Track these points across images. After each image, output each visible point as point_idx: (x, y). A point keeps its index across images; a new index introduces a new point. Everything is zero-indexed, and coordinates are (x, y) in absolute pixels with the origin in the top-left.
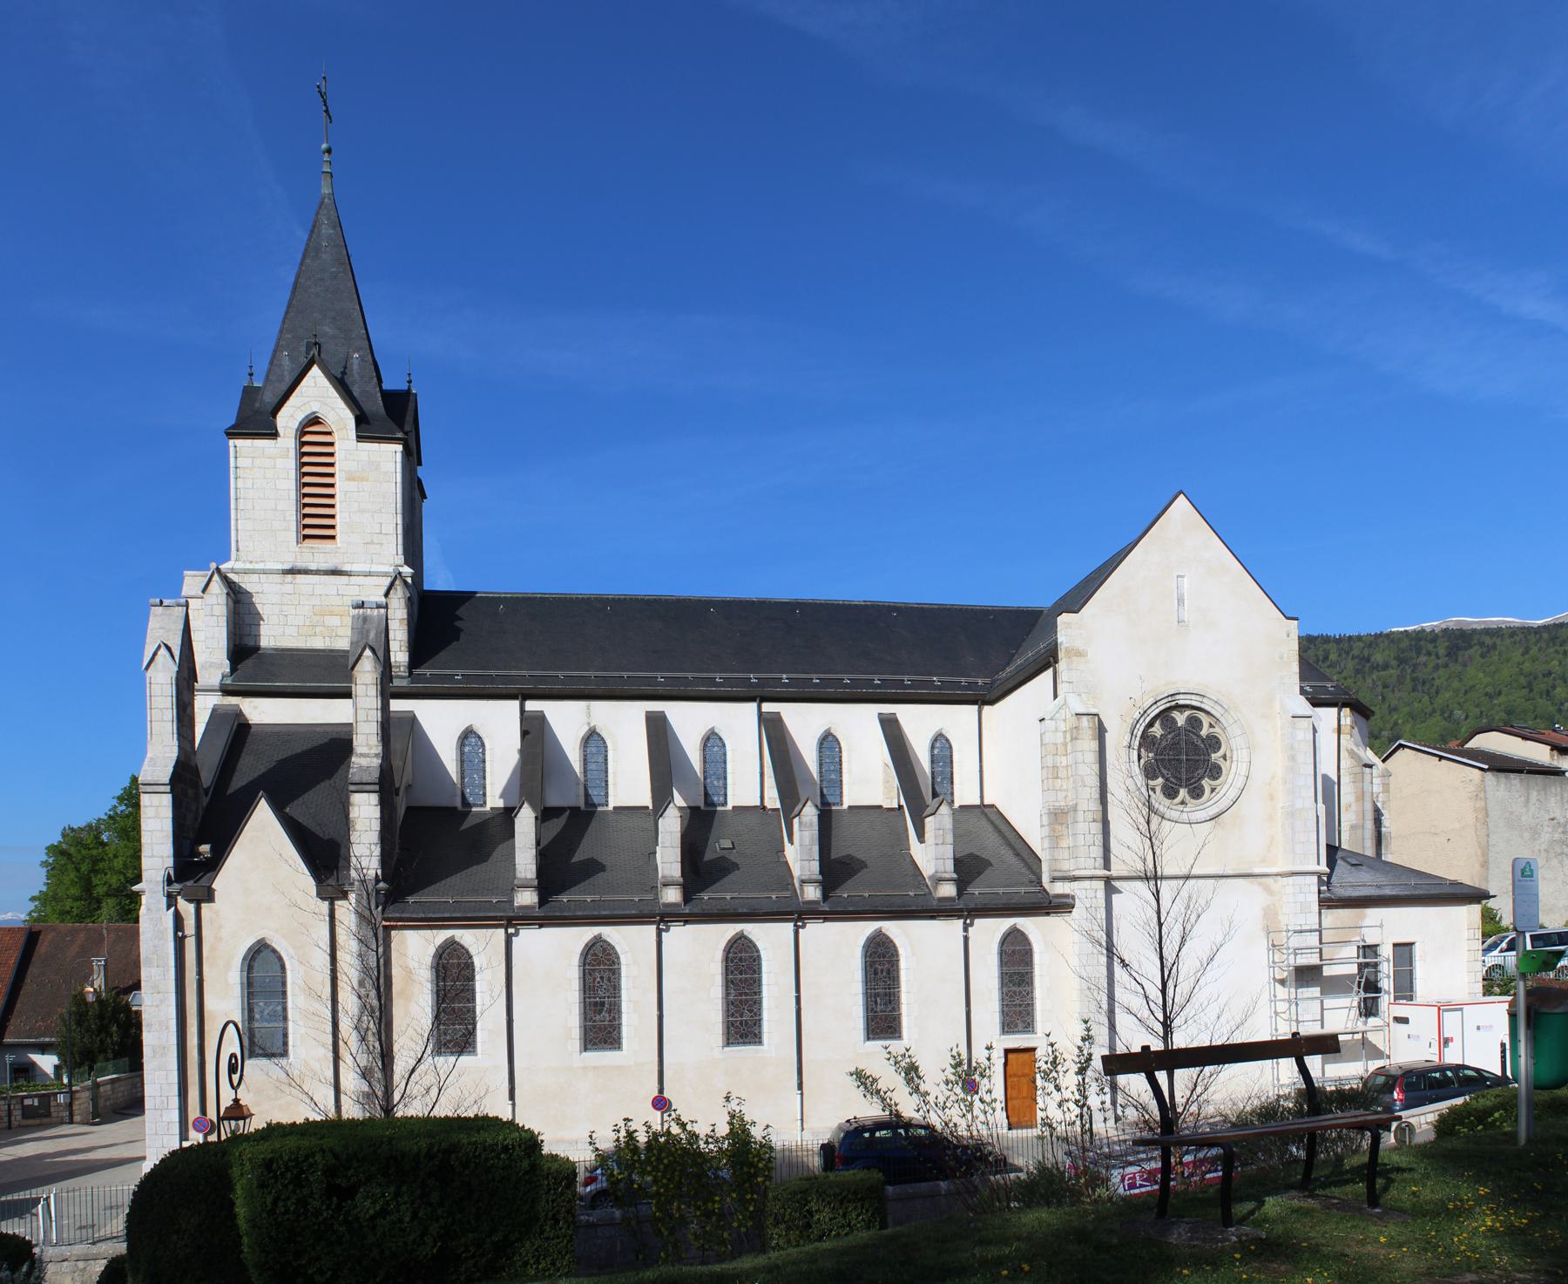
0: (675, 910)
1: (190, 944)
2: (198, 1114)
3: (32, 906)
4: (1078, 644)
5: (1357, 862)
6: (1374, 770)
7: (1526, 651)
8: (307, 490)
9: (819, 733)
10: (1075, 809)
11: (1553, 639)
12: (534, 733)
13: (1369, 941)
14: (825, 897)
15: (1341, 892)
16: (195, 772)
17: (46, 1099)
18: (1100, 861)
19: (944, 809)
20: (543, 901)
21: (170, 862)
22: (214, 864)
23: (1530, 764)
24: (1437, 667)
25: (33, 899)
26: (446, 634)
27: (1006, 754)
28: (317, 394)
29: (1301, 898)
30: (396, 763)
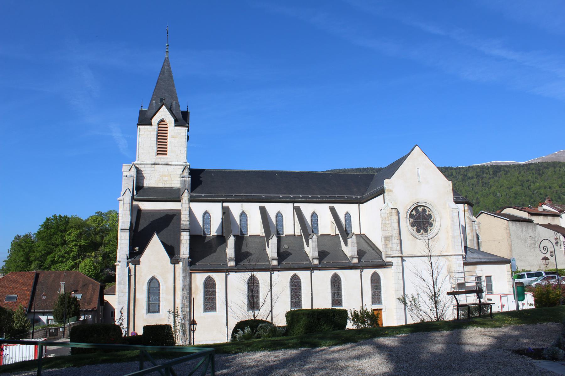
0: (276, 267)
2: (132, 331)
4: (390, 188)
5: (473, 251)
7: (520, 173)
9: (311, 213)
10: (392, 236)
11: (528, 169)
12: (226, 212)
13: (479, 275)
14: (279, 264)
15: (469, 260)
18: (400, 252)
21: (128, 253)
22: (141, 253)
23: (522, 218)
24: (490, 178)
26: (201, 183)
27: (369, 219)
28: (164, 113)
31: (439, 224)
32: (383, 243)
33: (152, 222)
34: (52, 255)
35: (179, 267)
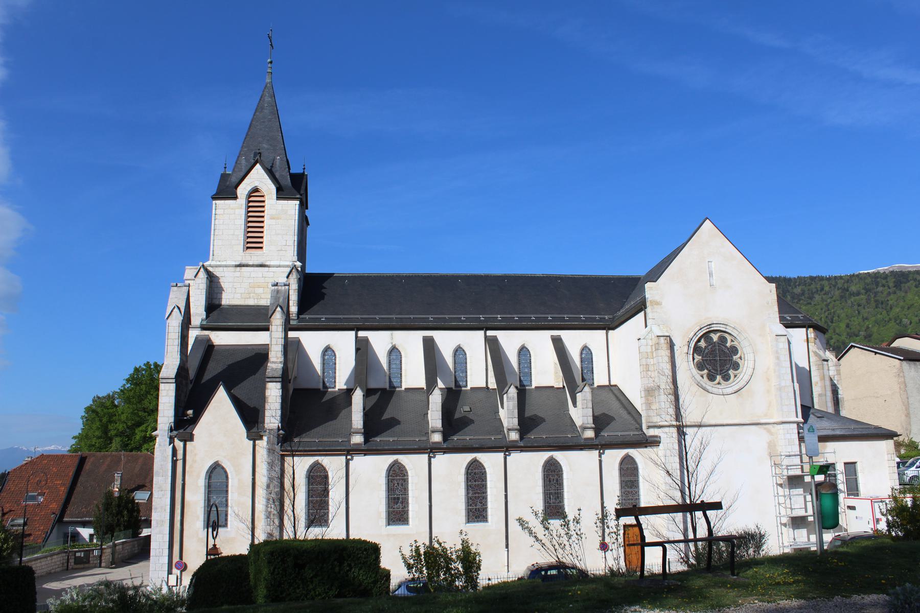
0: (438, 446)
3: (74, 442)
4: (657, 298)
5: (822, 415)
6: (830, 363)
8: (250, 224)
12: (363, 348)
14: (521, 438)
16: (187, 371)
17: (88, 553)
19: (587, 389)
20: (366, 441)
21: (172, 420)
22: (195, 420)
24: (889, 294)
25: (74, 438)
26: (318, 296)
27: (621, 357)
28: (258, 177)
29: (788, 436)
30: (290, 365)
31: (751, 365)
32: (643, 400)
33: (229, 366)
34: (143, 427)
35: (262, 444)
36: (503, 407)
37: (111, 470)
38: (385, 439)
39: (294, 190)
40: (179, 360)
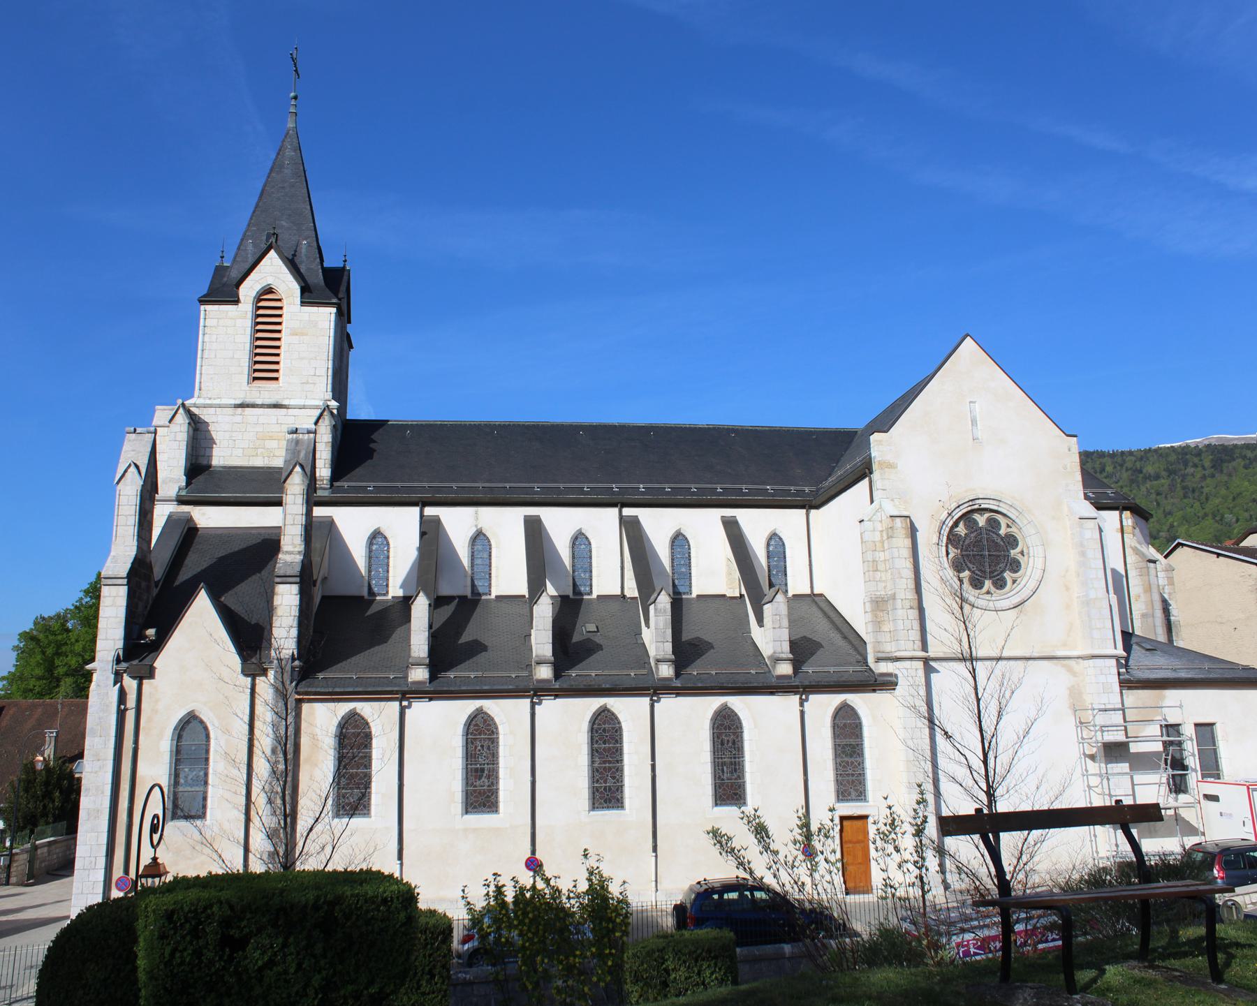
0: (546, 686)
1: (130, 717)
2: (121, 874)
4: (889, 458)
5: (1152, 647)
9: (671, 533)
10: (894, 597)
12: (431, 533)
13: (1171, 721)
14: (678, 674)
16: (150, 567)
18: (919, 644)
20: (433, 677)
21: (120, 644)
22: (157, 646)
24: (1204, 478)
26: (362, 454)
27: (832, 551)
28: (272, 271)
29: (1102, 679)
30: (316, 559)
31: (1039, 563)
32: (869, 617)
36: (648, 626)
37: (42, 725)
38: (458, 674)
39: (328, 292)
40: (135, 548)
